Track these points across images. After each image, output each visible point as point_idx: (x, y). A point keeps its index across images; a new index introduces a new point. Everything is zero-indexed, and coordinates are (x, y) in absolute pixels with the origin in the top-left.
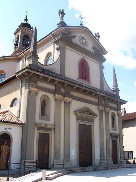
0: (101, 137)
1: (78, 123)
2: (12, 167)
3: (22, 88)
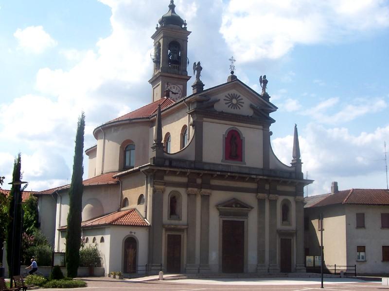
1: (221, 219)
2: (139, 268)
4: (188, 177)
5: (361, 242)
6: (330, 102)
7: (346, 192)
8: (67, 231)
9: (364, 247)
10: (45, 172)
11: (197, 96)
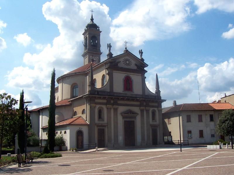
0: (142, 127)
1: (124, 120)
2: (85, 146)
3: (87, 104)
4: (107, 99)
5: (189, 129)
6: (160, 66)
7: (181, 106)
8: (48, 128)
9: (191, 131)
10: (38, 98)
11: (110, 60)
